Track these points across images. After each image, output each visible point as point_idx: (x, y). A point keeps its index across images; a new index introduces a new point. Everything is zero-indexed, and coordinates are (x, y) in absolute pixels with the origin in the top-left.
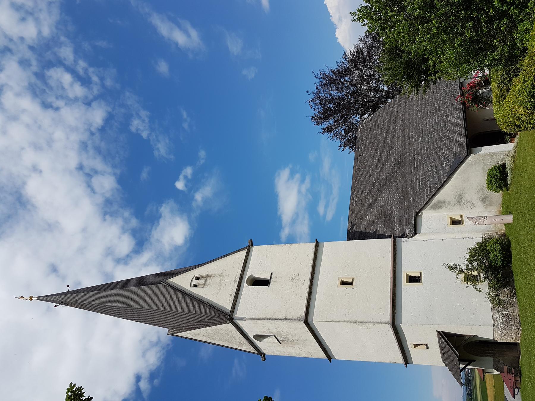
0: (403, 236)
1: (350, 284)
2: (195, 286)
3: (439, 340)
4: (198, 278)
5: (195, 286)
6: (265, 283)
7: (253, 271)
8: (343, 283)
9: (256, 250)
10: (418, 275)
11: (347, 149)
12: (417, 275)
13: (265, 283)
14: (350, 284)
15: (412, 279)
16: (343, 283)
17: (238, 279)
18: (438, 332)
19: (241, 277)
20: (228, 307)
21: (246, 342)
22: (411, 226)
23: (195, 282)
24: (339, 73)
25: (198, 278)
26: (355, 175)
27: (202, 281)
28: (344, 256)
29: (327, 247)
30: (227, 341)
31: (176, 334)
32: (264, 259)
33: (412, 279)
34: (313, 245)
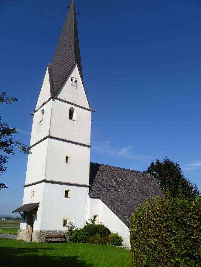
0: (90, 189)
1: (67, 161)
2: (72, 80)
3: (35, 203)
4: (76, 82)
5: (72, 80)
6: (71, 117)
7: (76, 110)
8: (67, 158)
9: (90, 113)
10: (69, 196)
11: (122, 244)
12: (69, 196)
13: (71, 117)
14: (67, 161)
15: (66, 194)
16: (67, 158)
17: (74, 103)
18: (39, 203)
19: (75, 105)
20: (59, 97)
21: (41, 105)
22: (94, 195)
23: (74, 80)
24: (172, 208)
25: (76, 82)
26: (125, 170)
27: (74, 83)
28: (82, 159)
29: (89, 149)
30: (34, 122)
31: (36, 110)
32: (84, 117)
33: (66, 194)
34: (89, 144)
